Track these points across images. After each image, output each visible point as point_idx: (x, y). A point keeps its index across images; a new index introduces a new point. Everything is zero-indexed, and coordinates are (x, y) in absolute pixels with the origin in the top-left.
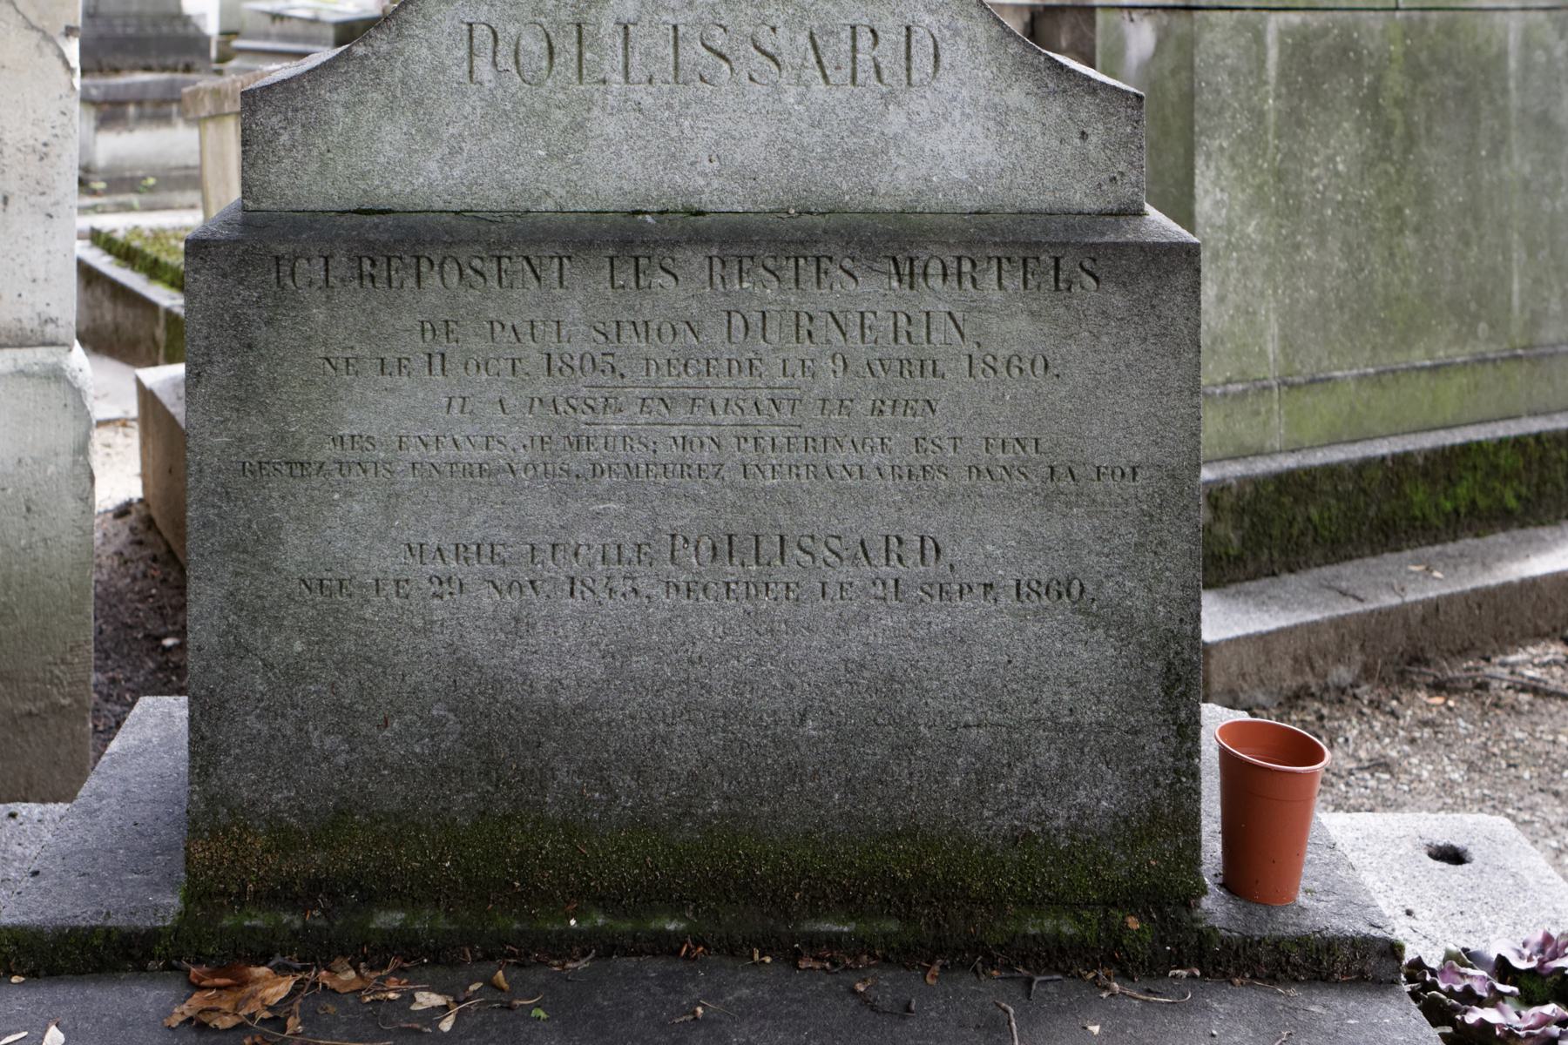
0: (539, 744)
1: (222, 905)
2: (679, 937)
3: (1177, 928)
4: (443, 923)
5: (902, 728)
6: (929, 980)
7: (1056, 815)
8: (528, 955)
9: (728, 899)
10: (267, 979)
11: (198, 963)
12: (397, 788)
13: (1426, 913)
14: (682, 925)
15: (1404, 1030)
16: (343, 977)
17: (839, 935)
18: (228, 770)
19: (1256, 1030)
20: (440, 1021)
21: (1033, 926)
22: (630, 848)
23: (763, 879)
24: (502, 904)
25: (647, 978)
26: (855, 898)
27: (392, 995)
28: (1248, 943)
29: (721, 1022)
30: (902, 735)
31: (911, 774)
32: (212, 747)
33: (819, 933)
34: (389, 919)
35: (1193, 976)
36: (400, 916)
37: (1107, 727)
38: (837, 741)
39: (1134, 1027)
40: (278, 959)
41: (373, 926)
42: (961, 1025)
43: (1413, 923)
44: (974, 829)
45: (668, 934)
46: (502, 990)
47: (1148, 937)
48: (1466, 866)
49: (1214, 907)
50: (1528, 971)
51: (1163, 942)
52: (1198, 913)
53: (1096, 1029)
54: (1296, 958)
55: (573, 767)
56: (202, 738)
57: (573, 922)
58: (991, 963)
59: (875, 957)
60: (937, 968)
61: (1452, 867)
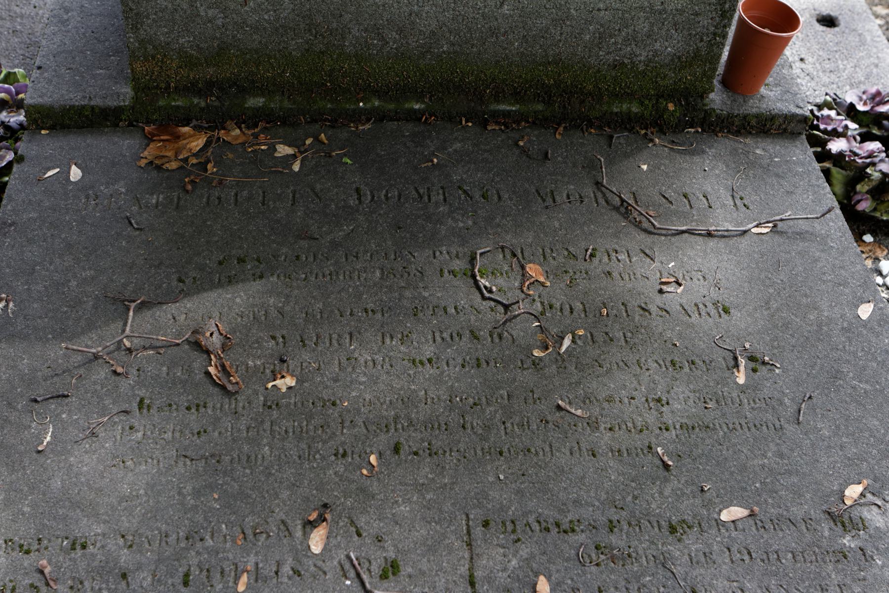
0: (341, 16)
1: (157, 93)
2: (421, 112)
3: (694, 110)
4: (287, 104)
5: (560, 10)
6: (557, 136)
7: (641, 55)
8: (336, 121)
9: (449, 92)
10: (191, 136)
11: (148, 123)
12: (255, 37)
13: (810, 60)
14: (423, 106)
15: (803, 164)
16: (233, 133)
17: (509, 112)
18: (150, 27)
19: (727, 166)
20: (292, 164)
21: (617, 107)
22: (394, 67)
23: (469, 83)
24: (320, 94)
25: (404, 136)
26: (520, 92)
27: (263, 147)
28: (730, 116)
29: (447, 166)
30: (559, 14)
31: (561, 34)
32: (137, 14)
33: (499, 111)
34: (256, 102)
35: (697, 132)
36: (262, 100)
37: (681, 12)
38: (520, 16)
39: (665, 165)
40: (194, 122)
41: (247, 106)
42: (575, 165)
43: (803, 66)
44: (592, 61)
45: (415, 111)
46: (324, 144)
47: (678, 114)
48: (836, 29)
49: (717, 98)
50: (864, 112)
51: (685, 115)
52: (707, 101)
53: (645, 167)
54: (754, 122)
55: (361, 27)
56: (131, 9)
57: (361, 104)
58: (590, 125)
59: (528, 122)
60: (562, 128)
61: (828, 29)
